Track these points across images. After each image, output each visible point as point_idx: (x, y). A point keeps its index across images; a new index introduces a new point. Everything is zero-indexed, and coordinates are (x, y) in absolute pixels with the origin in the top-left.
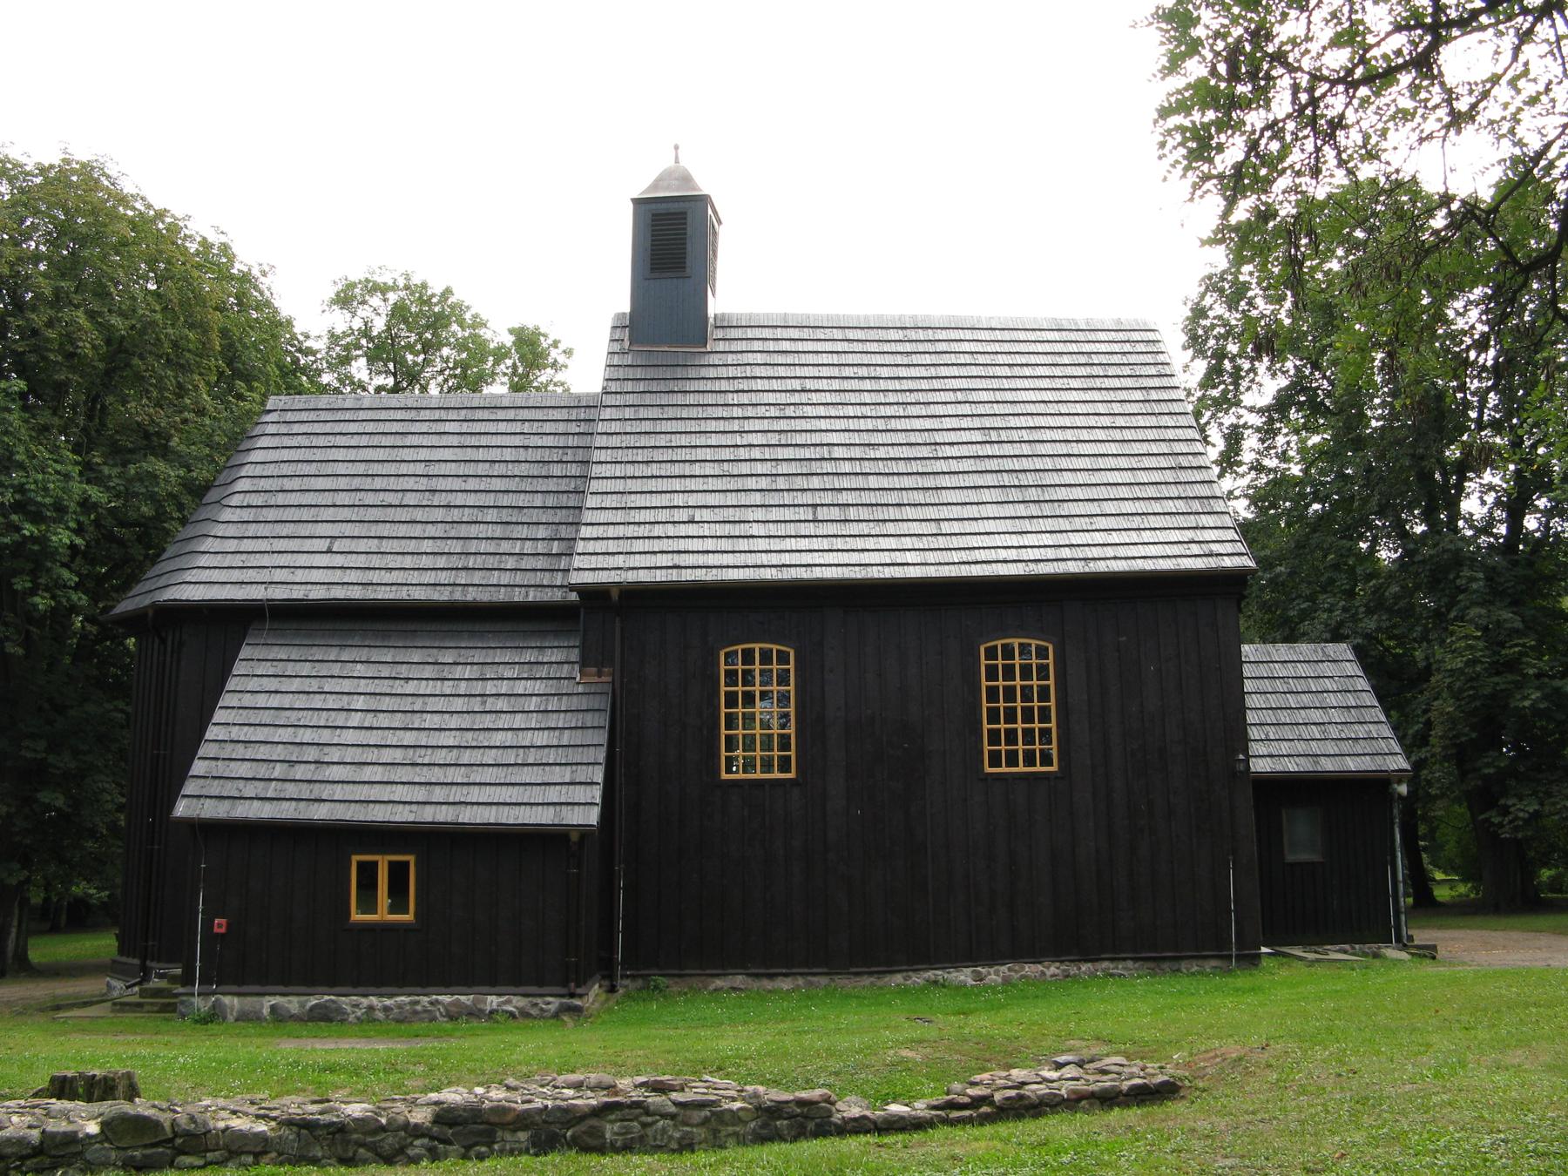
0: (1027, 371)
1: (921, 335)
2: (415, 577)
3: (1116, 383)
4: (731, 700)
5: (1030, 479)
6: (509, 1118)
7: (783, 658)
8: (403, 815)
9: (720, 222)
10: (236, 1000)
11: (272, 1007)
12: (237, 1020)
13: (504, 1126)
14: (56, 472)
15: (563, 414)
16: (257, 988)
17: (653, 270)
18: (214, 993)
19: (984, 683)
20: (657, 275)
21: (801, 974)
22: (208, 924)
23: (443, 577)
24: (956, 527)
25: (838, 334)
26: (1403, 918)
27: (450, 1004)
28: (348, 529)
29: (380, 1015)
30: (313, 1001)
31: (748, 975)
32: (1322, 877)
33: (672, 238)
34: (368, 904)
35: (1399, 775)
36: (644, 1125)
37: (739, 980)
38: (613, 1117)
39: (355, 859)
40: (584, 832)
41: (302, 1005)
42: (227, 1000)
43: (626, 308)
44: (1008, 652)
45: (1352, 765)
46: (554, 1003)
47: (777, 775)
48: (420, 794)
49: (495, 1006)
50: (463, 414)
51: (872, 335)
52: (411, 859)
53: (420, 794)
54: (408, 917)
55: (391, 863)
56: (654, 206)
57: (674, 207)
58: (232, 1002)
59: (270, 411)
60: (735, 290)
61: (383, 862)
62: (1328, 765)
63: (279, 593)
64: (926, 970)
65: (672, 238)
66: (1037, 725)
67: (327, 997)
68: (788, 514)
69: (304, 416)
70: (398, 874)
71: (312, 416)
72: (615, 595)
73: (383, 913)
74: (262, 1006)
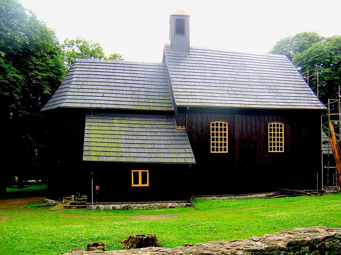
2: (128, 103)
3: (137, 86)
6: (305, 243)
7: (213, 125)
8: (146, 160)
10: (103, 205)
11: (113, 207)
12: (103, 210)
13: (303, 246)
14: (13, 73)
15: (154, 67)
17: (176, 33)
18: (97, 204)
19: (269, 132)
22: (94, 187)
27: (159, 205)
28: (106, 91)
30: (123, 205)
31: (216, 196)
33: (180, 26)
34: (136, 182)
36: (334, 242)
38: (327, 240)
39: (133, 171)
41: (121, 207)
42: (100, 206)
43: (169, 43)
44: (274, 126)
47: (223, 152)
49: (170, 205)
51: (227, 54)
52: (148, 171)
54: (147, 185)
55: (142, 172)
56: (176, 17)
57: (181, 18)
58: (102, 206)
59: (77, 62)
60: (196, 39)
61: (140, 172)
63: (94, 106)
64: (255, 194)
65: (180, 26)
66: (223, 142)
67: (127, 205)
68: (223, 92)
69: (86, 64)
71: (89, 64)
72: (188, 108)
73: (140, 184)
74: (110, 207)
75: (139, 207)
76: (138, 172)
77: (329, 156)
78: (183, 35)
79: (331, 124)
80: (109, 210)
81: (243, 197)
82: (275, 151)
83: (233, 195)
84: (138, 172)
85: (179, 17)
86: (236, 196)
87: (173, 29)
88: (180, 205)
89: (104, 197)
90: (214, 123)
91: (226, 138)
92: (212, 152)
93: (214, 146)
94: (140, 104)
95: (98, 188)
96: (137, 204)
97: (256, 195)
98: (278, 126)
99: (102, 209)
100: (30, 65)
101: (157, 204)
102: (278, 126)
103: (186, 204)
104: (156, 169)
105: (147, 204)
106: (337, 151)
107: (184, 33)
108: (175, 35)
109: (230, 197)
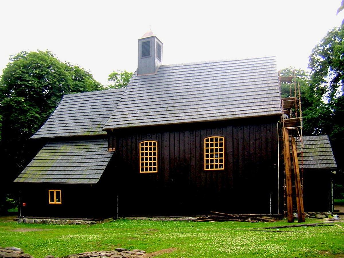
0: (235, 70)
1: (210, 65)
4: (221, 161)
5: (226, 96)
8: (58, 181)
9: (162, 44)
10: (28, 219)
16: (32, 217)
20: (143, 57)
21: (158, 217)
22: (22, 204)
23: (86, 130)
24: (202, 109)
25: (188, 67)
26: (333, 206)
29: (55, 223)
30: (42, 220)
31: (146, 217)
32: (319, 194)
34: (53, 201)
35: (334, 169)
37: (144, 218)
39: (49, 190)
40: (94, 185)
41: (40, 220)
42: (26, 219)
44: (212, 140)
45: (319, 166)
46: (90, 222)
47: (153, 172)
48: (63, 177)
50: (102, 95)
53: (63, 177)
55: (56, 192)
56: (142, 41)
58: (27, 220)
60: (169, 58)
61: (55, 191)
62: (312, 167)
64: (188, 217)
65: (147, 48)
67: (44, 219)
70: (58, 193)
72: (112, 130)
73: (55, 202)
75: (53, 222)
76: (53, 191)
77: (303, 170)
78: (149, 56)
79: (286, 131)
80: (32, 223)
81: (175, 219)
82: (213, 168)
83: (164, 216)
84: (53, 191)
85: (145, 40)
86: (166, 218)
87: (140, 53)
88: (86, 222)
89: (28, 212)
90: (209, 139)
91: (156, 157)
92: (141, 172)
93: (148, 166)
94: (93, 130)
95: (24, 204)
96: (52, 219)
97: (189, 218)
98: (216, 140)
99: (27, 222)
100: (50, 104)
101: (66, 220)
102: (216, 140)
103: (91, 222)
104: (67, 189)
105: (59, 220)
106: (288, 166)
107: (149, 55)
108: (142, 59)
109: (160, 218)
